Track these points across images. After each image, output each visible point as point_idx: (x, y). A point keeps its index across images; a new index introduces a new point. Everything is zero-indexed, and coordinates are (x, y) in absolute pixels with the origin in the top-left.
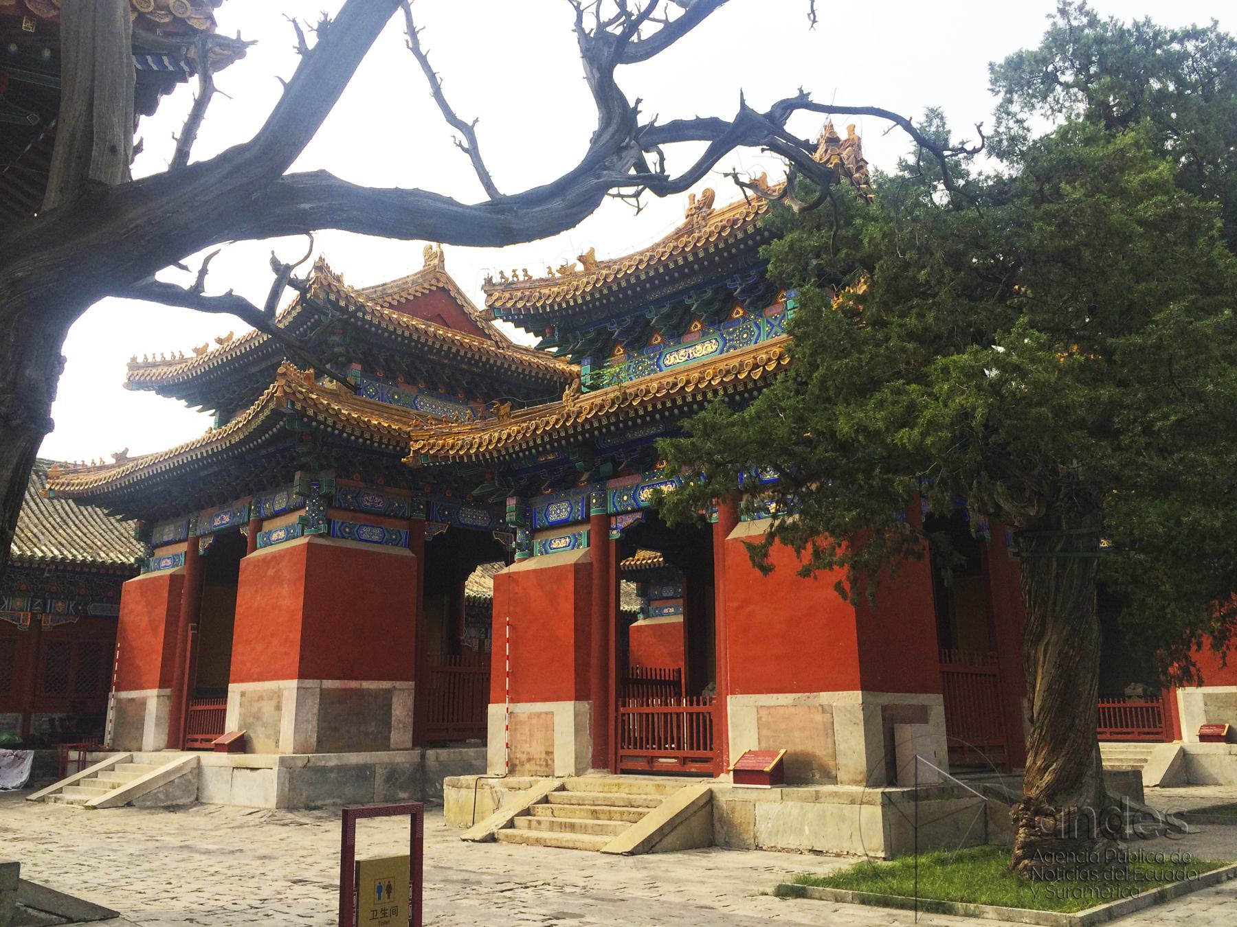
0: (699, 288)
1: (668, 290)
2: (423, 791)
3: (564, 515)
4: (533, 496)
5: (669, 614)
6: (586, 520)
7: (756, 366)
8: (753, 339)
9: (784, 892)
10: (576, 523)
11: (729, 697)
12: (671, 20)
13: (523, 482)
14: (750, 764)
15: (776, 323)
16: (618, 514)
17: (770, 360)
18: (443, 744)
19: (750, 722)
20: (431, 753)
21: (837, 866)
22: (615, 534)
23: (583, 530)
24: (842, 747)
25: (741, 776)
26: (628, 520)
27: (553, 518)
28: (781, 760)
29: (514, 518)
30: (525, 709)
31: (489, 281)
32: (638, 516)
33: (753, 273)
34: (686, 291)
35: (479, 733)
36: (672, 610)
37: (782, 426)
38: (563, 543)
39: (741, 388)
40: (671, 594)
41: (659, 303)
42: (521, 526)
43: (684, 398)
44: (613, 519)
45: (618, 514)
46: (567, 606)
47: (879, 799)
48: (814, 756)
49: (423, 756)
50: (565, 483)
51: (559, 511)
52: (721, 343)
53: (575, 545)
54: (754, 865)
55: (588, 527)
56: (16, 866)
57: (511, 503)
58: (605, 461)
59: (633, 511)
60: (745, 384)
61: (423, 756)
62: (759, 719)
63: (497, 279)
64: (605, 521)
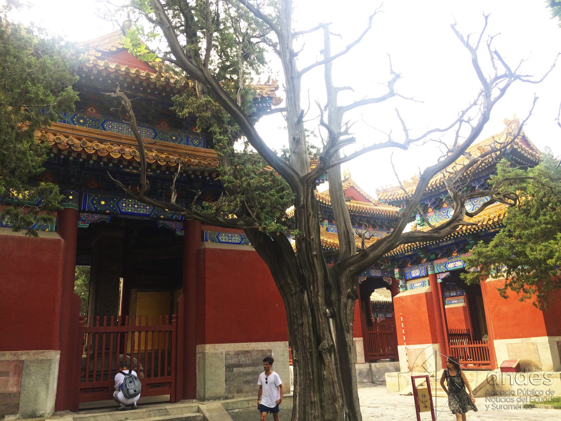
2: (372, 379)
3: (418, 274)
4: (404, 267)
5: (455, 303)
6: (427, 276)
7: (490, 219)
9: (526, 407)
10: (423, 277)
11: (494, 341)
12: (465, 164)
13: (400, 263)
14: (507, 365)
16: (439, 273)
17: (495, 217)
18: (375, 361)
19: (504, 350)
20: (373, 365)
22: (439, 281)
23: (427, 279)
24: (542, 357)
25: (504, 369)
26: (444, 275)
27: (413, 275)
28: (519, 363)
29: (398, 276)
30: (412, 347)
31: (377, 190)
32: (448, 273)
33: (482, 180)
35: (395, 358)
36: (456, 301)
37: (504, 250)
38: (419, 284)
39: (484, 227)
40: (455, 294)
42: (401, 279)
43: (462, 232)
44: (438, 275)
45: (439, 273)
46: (424, 308)
47: (559, 376)
48: (532, 362)
49: (370, 366)
50: (415, 261)
51: (415, 273)
52: (472, 206)
53: (424, 285)
55: (428, 278)
57: (396, 271)
58: (431, 254)
59: (446, 272)
60: (486, 226)
61: (370, 366)
62: (508, 348)
63: (380, 189)
64: (435, 276)
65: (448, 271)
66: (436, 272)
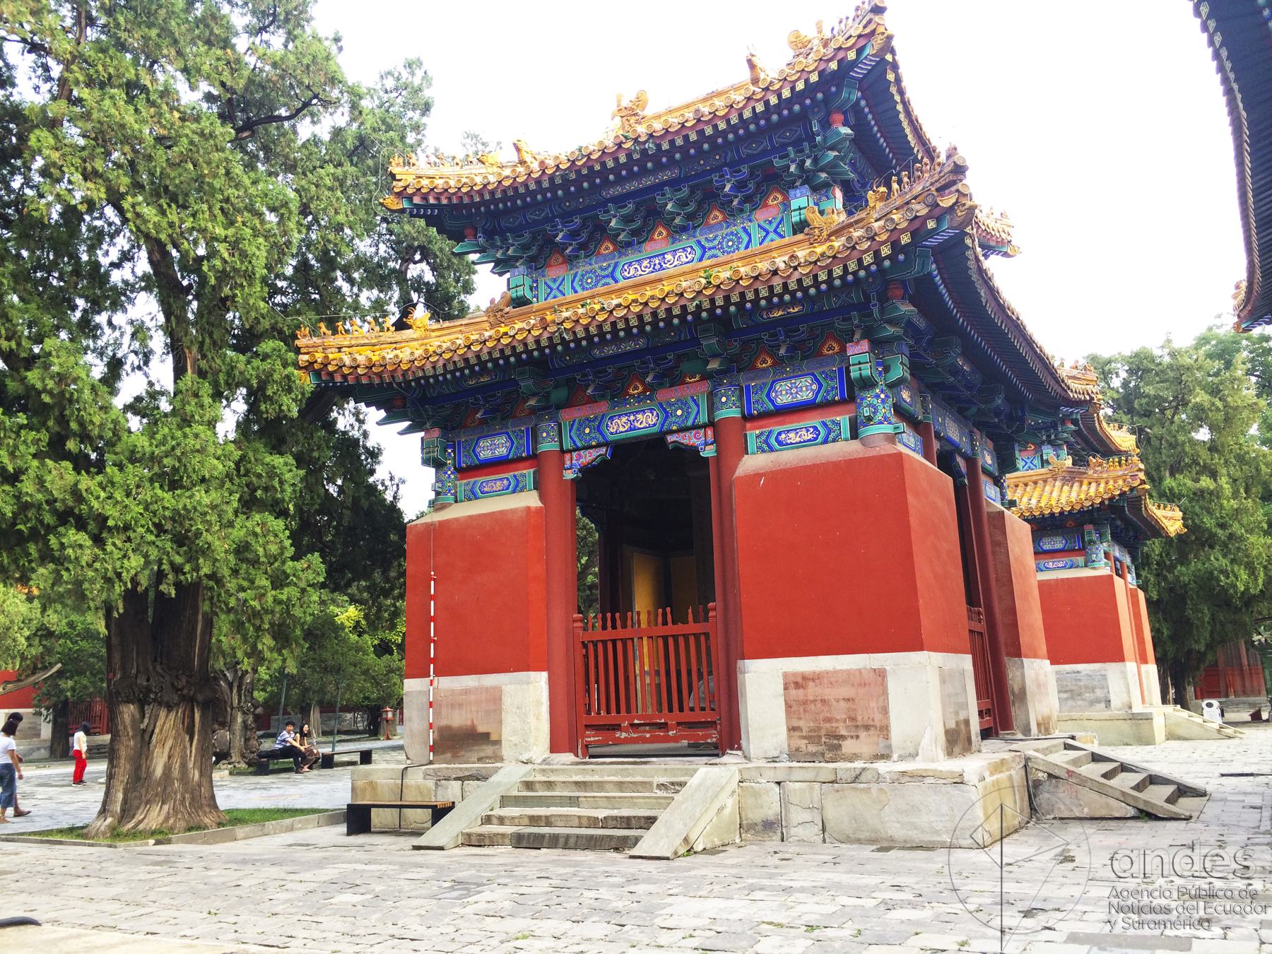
0: (674, 184)
1: (633, 186)
3: (502, 451)
5: (498, 493)
8: (742, 246)
15: (771, 228)
21: (910, 833)
26: (588, 457)
34: (659, 187)
41: (620, 201)
54: (1147, 827)
56: (349, 833)
59: (599, 446)
65: (606, 444)
66: (568, 444)
